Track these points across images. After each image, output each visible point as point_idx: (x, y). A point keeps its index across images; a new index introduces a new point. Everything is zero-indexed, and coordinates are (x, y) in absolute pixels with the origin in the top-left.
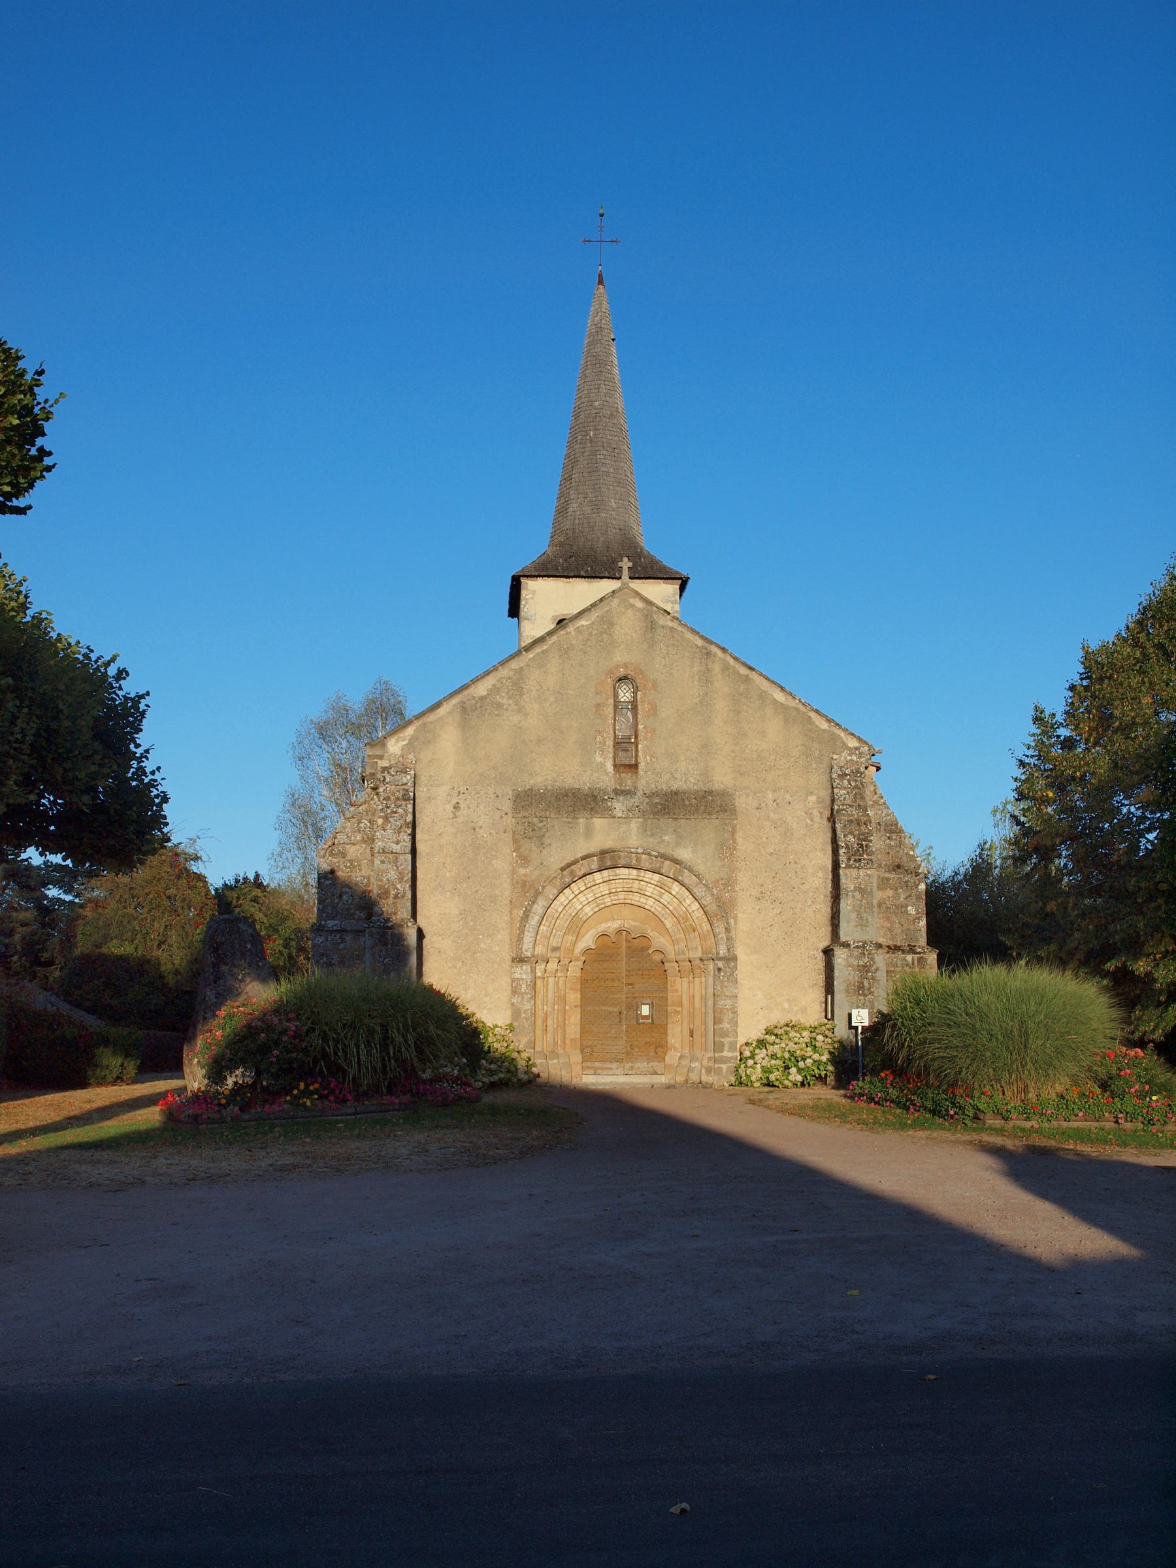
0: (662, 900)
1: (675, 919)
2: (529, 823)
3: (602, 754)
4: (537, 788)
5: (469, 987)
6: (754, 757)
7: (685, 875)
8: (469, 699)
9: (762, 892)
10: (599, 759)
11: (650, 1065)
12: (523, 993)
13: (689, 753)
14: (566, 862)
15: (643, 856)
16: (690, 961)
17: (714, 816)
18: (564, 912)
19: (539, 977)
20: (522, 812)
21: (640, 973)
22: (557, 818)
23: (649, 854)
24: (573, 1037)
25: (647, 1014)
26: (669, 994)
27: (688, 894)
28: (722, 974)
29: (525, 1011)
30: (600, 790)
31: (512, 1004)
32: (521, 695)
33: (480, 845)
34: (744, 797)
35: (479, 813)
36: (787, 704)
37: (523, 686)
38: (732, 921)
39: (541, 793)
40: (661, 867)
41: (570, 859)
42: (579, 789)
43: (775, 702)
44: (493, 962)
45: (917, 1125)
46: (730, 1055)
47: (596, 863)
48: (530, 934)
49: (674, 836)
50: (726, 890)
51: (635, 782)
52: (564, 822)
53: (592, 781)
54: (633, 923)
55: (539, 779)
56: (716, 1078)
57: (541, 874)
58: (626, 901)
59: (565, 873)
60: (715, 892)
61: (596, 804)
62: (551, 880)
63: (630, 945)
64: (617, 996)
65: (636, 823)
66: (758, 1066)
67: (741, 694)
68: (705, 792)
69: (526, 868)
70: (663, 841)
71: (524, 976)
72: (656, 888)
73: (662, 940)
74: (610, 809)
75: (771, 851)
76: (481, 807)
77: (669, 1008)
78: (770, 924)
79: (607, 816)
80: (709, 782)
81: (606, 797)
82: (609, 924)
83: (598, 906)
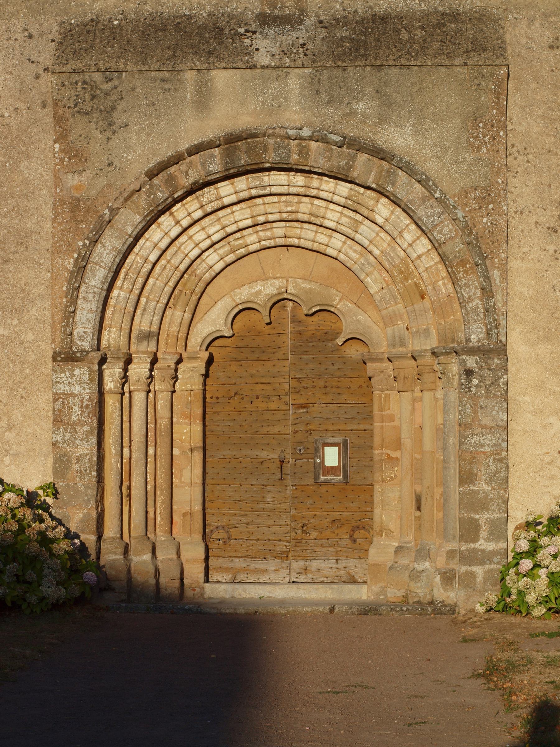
0: (358, 237)
1: (385, 275)
2: (85, 82)
4: (107, 17)
7: (399, 183)
11: (341, 564)
12: (74, 423)
14: (158, 159)
15: (314, 145)
16: (414, 358)
17: (458, 61)
19: (111, 392)
20: (71, 62)
21: (321, 383)
23: (325, 140)
24: (187, 509)
25: (335, 463)
26: (377, 424)
27: (408, 221)
28: (475, 382)
29: (78, 459)
30: (231, 16)
31: (54, 444)
34: (523, 25)
38: (496, 274)
39: (113, 27)
40: (350, 167)
42: (190, 17)
44: (22, 363)
46: (490, 546)
47: (218, 160)
48: (87, 306)
52: (155, 80)
54: (306, 286)
56: (462, 593)
57: (109, 185)
58: (289, 241)
59: (156, 181)
60: (460, 215)
61: (221, 43)
63: (301, 328)
64: (276, 430)
65: (300, 76)
68: (444, 14)
69: (80, 172)
70: (354, 113)
71: (77, 389)
72: (346, 211)
73: (362, 317)
77: (376, 452)
81: (242, 30)
82: (258, 287)
83: (233, 251)
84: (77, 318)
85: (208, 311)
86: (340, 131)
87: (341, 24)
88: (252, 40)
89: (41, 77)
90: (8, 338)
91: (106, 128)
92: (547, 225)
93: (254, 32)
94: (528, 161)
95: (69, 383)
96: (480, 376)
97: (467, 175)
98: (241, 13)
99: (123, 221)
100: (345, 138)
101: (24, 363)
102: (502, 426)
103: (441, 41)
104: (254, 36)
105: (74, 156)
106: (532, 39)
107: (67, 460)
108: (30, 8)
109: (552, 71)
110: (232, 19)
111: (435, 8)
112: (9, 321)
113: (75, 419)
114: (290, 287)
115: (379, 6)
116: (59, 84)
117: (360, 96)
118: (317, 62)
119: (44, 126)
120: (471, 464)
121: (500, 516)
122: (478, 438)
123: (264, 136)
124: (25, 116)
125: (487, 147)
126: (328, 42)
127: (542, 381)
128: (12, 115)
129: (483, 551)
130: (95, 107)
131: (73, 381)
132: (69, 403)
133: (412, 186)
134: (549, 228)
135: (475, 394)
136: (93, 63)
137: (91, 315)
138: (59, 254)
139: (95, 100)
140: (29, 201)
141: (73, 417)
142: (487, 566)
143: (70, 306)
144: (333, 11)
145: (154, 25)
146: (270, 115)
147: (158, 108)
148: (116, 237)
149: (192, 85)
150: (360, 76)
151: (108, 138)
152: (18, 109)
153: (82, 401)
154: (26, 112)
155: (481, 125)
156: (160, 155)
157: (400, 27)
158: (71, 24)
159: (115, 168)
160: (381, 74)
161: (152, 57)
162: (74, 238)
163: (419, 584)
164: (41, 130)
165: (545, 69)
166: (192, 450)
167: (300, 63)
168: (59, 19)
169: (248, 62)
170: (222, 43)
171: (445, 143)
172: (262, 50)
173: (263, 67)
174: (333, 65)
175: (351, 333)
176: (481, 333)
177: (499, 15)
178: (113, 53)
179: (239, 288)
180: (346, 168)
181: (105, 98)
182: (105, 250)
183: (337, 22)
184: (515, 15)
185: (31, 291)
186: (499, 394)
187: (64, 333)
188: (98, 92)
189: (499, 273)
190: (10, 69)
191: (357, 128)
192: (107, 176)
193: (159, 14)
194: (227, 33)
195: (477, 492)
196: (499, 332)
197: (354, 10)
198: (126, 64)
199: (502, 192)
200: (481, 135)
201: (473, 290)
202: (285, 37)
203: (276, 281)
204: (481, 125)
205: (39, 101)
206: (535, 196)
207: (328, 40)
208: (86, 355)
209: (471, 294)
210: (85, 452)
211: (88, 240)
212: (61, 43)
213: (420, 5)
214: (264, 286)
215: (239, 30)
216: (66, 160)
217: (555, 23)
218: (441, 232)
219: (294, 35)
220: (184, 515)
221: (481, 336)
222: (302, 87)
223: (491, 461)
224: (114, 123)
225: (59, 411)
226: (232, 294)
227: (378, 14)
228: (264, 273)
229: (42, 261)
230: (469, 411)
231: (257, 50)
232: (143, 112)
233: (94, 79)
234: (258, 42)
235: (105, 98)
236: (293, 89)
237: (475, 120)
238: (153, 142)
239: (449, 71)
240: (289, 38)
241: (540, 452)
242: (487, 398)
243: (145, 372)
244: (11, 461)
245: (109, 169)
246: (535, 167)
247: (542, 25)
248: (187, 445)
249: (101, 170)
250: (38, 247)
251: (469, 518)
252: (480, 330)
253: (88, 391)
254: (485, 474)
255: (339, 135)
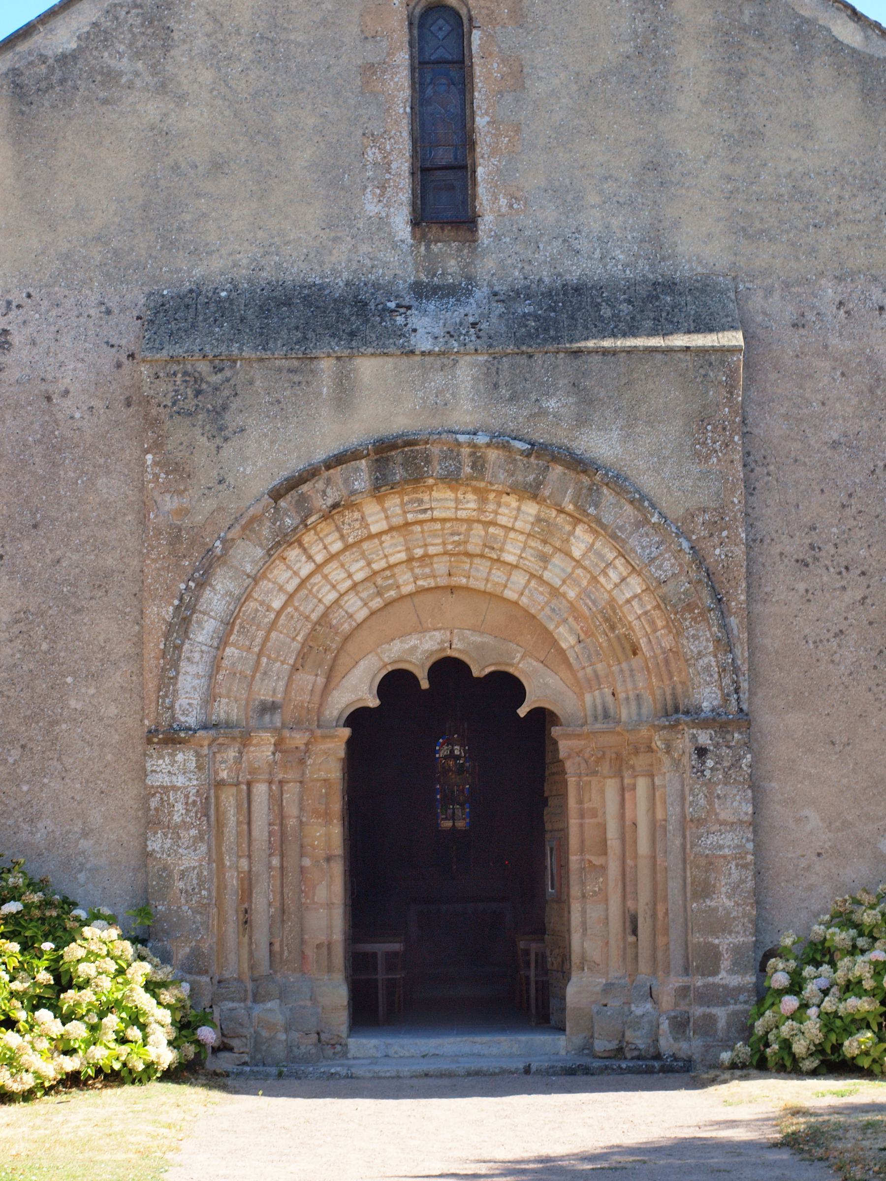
0: (547, 575)
2: (185, 373)
3: (382, 195)
5: (40, 813)
6: (783, 190)
7: (604, 503)
8: (31, 63)
9: (811, 546)
10: (372, 208)
12: (177, 826)
13: (609, 187)
14: (285, 474)
18: (290, 609)
22: (261, 360)
23: (506, 447)
28: (710, 763)
29: (183, 875)
30: (377, 286)
32: (166, 48)
33: (63, 438)
35: (61, 357)
36: (868, 51)
37: (171, 24)
39: (220, 301)
41: (295, 464)
42: (322, 288)
43: (837, 46)
44: (102, 746)
45: (398, 436)
46: (734, 981)
47: (365, 475)
48: (192, 669)
49: (571, 400)
50: (716, 540)
51: (468, 264)
52: (280, 370)
53: (354, 266)
54: (477, 639)
55: (216, 264)
57: (220, 509)
59: (283, 503)
62: (250, 526)
65: (473, 365)
66: (813, 1012)
67: (744, 29)
70: (543, 413)
71: (180, 781)
73: (552, 680)
74: (400, 333)
75: (835, 436)
76: (66, 340)
78: (835, 629)
79: (392, 349)
80: (663, 259)
81: (392, 305)
82: (413, 641)
84: (179, 685)
85: (346, 674)
86: (526, 437)
87: (522, 296)
88: (406, 318)
89: (124, 367)
90: (82, 712)
91: (215, 434)
92: (795, 557)
93: (409, 308)
94: (768, 474)
95: (169, 772)
96: (716, 755)
97: (693, 493)
98: (389, 282)
99: (239, 557)
100: (533, 445)
101: (104, 746)
102: (745, 822)
103: (654, 319)
104: (409, 312)
105: (172, 471)
106: (770, 315)
107: (168, 875)
108: (107, 275)
109: (797, 356)
110: (379, 289)
111: (644, 276)
112: (83, 690)
113: (178, 820)
114: (455, 641)
115: (571, 272)
116: (151, 375)
117: (551, 391)
118: (495, 347)
119: (129, 431)
120: (706, 872)
121: (746, 940)
122: (715, 838)
123: (427, 443)
124: (103, 418)
125: (718, 457)
126: (507, 320)
127: (794, 761)
128: (86, 416)
129: (725, 987)
130: (201, 405)
131: (174, 769)
132: (169, 799)
133: (621, 508)
134: (797, 561)
135: (710, 780)
136: (197, 348)
137: (197, 681)
138: (153, 600)
139: (200, 397)
140: (109, 530)
141: (175, 818)
142: (731, 1007)
143: (170, 669)
144: (511, 279)
145: (275, 297)
146: (434, 416)
147: (285, 407)
148: (230, 578)
149: (329, 377)
150: (551, 364)
151: (218, 447)
152: (93, 407)
153: (187, 797)
154: (105, 413)
155: (709, 427)
156: (288, 468)
157: (599, 300)
158: (163, 296)
159: (229, 486)
160: (578, 362)
161: (276, 340)
162: (174, 579)
163: (638, 1033)
164: (124, 435)
165: (787, 354)
166: (328, 859)
167: (472, 347)
168: (146, 289)
169: (403, 346)
170: (368, 321)
171: (664, 451)
172: (421, 331)
173: (423, 353)
174: (516, 351)
175: (537, 701)
176: (716, 699)
177: (727, 285)
178: (223, 335)
179: (388, 643)
180: (534, 484)
181: (214, 394)
182: (215, 594)
183: (517, 294)
184: (747, 285)
185: (113, 650)
186: (741, 779)
187: (162, 705)
188: (204, 386)
189: (737, 621)
190: (82, 355)
191: (549, 433)
192: (217, 497)
193: (280, 283)
194: (373, 308)
195: (716, 909)
196: (739, 698)
197: (537, 278)
198: (241, 349)
199: (739, 515)
200: (709, 441)
201: (704, 643)
202: (450, 313)
203: (437, 633)
204: (709, 427)
205: (121, 397)
206: (778, 519)
207: (506, 317)
208: (193, 735)
209: (702, 648)
210: (192, 865)
211: (193, 581)
212: (151, 322)
213: (625, 271)
214: (420, 639)
215: (389, 304)
216: (162, 475)
217: (800, 295)
218: (660, 567)
219: (462, 311)
220: (319, 946)
221: (715, 703)
222: (475, 379)
223: (733, 867)
224: (227, 428)
225: (157, 809)
226: (379, 650)
227: (570, 283)
228: (420, 623)
229: (128, 610)
230: (703, 802)
231: (415, 330)
232: (264, 412)
233: (199, 369)
234: (415, 320)
235: (214, 394)
236: (462, 382)
237: (702, 421)
238: (279, 451)
239: (667, 359)
240: (455, 315)
241: (793, 855)
242: (726, 785)
243: (268, 756)
244: (88, 878)
245: (220, 487)
246: (777, 480)
247: (783, 298)
248: (321, 853)
249: (210, 488)
250: (122, 592)
251: (706, 943)
252: (714, 695)
253: (195, 783)
254: (726, 884)
255: (525, 442)
